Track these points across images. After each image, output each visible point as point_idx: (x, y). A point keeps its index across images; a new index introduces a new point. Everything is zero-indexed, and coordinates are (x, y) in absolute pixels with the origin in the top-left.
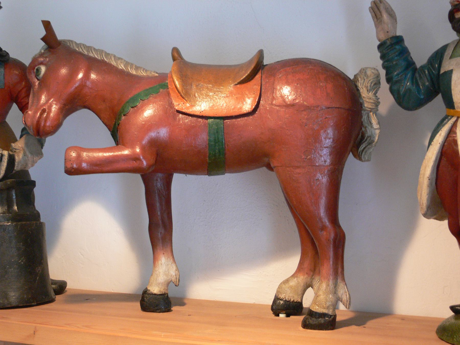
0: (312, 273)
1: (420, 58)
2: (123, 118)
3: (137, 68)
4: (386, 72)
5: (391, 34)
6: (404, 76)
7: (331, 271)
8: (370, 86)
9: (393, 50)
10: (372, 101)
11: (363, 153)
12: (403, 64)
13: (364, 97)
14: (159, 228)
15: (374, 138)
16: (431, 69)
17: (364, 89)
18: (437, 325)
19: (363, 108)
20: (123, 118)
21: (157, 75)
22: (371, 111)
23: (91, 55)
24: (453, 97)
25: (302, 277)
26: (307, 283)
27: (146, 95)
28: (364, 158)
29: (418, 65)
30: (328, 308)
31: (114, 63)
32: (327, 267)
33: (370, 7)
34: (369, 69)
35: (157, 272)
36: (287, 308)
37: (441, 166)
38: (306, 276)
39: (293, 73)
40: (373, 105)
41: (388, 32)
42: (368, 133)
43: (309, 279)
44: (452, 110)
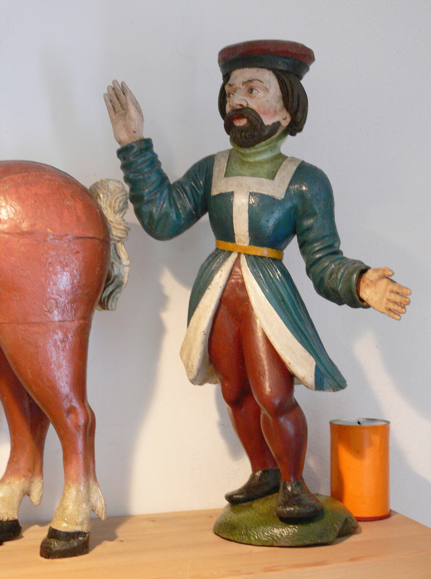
0: (30, 475)
1: (176, 165)
5: (137, 137)
6: (158, 195)
8: (119, 206)
9: (137, 157)
10: (122, 227)
11: (111, 299)
12: (154, 178)
13: (111, 221)
15: (123, 278)
16: (195, 189)
17: (109, 209)
19: (111, 236)
22: (119, 241)
24: (235, 227)
25: (17, 482)
26: (24, 490)
28: (111, 306)
29: (172, 180)
30: (82, 523)
33: (105, 94)
34: (111, 182)
37: (219, 317)
38: (23, 479)
39: (24, 184)
40: (124, 232)
41: (134, 132)
42: (116, 272)
43: (26, 484)
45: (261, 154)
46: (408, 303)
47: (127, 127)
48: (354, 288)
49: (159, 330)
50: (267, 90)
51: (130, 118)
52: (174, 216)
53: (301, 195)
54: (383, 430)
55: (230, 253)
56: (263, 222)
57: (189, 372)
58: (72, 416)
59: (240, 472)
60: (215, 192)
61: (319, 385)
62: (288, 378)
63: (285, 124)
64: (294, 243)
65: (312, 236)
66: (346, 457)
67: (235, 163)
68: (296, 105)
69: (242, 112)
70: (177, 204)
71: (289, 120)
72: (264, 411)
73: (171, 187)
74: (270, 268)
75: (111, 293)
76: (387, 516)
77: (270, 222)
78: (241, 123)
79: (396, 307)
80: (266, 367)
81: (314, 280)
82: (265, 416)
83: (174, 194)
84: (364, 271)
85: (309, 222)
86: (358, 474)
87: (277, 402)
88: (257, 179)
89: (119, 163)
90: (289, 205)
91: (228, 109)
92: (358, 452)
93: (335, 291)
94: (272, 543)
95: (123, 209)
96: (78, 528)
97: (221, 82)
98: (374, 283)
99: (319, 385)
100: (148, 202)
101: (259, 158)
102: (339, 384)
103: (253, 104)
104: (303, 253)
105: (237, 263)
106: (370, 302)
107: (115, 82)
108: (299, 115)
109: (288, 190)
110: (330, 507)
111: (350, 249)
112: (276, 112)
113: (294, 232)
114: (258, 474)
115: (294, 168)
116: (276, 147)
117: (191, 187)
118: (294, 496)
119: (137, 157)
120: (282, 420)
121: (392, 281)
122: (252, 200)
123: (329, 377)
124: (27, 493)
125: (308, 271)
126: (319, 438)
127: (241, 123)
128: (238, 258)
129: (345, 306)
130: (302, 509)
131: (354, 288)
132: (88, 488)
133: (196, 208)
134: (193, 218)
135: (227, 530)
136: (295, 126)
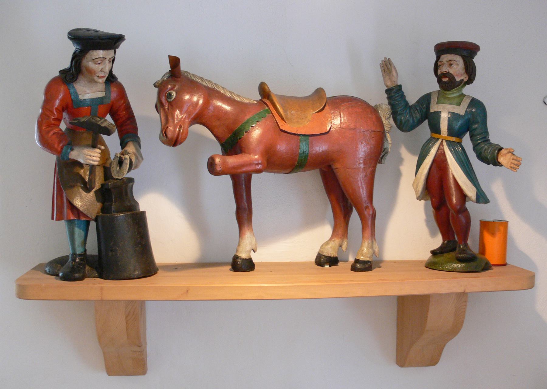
1: (412, 98)
2: (245, 133)
3: (238, 96)
4: (371, 106)
7: (370, 235)
9: (395, 94)
14: (244, 214)
18: (424, 264)
20: (245, 133)
21: (256, 102)
23: (204, 84)
27: (259, 118)
29: (410, 104)
31: (222, 91)
32: (368, 232)
35: (245, 243)
36: (325, 261)
44: (438, 135)
45: (453, 94)
46: (520, 164)
47: (391, 80)
48: (496, 157)
49: (399, 175)
50: (458, 65)
51: (393, 75)
52: (411, 121)
53: (472, 113)
54: (505, 224)
55: (438, 139)
56: (454, 125)
57: (417, 193)
58: (367, 210)
59: (438, 241)
60: (432, 111)
61: (478, 201)
62: (463, 197)
63: (465, 80)
64: (468, 135)
65: (476, 133)
66: (488, 237)
67: (442, 98)
68: (471, 71)
69: (446, 75)
70: (412, 114)
71: (467, 78)
72: (452, 211)
73: (411, 107)
74: (456, 146)
75: (383, 156)
76: (505, 265)
77: (457, 125)
78: (446, 80)
79: (515, 166)
80: (454, 192)
81: (476, 153)
82: (452, 213)
83: (412, 111)
84: (500, 149)
85: (475, 126)
86: (492, 244)
87: (458, 207)
88: (452, 106)
89: (386, 96)
90: (466, 118)
91: (439, 72)
92: (493, 234)
93: (487, 158)
94: (454, 271)
95: (389, 118)
96: (368, 259)
97: (435, 59)
98: (505, 155)
99: (478, 201)
100: (400, 114)
101: (452, 96)
102: (486, 201)
103: (451, 71)
104: (472, 140)
105: (441, 144)
106: (502, 164)
107: (385, 58)
108: (472, 76)
109: (466, 111)
110: (480, 256)
111: (494, 138)
112: (462, 75)
113: (468, 130)
114: (446, 242)
115: (469, 101)
116: (461, 90)
117: (420, 108)
118: (464, 250)
119: (395, 94)
120: (460, 216)
121: (514, 155)
122: (449, 116)
123: (482, 198)
124: (341, 246)
125: (474, 149)
126: (475, 227)
127: (446, 80)
128: (442, 142)
129: (491, 165)
130: (468, 256)
131: (496, 157)
132: (372, 242)
133: (422, 117)
134: (420, 122)
135: (431, 265)
136: (471, 80)
